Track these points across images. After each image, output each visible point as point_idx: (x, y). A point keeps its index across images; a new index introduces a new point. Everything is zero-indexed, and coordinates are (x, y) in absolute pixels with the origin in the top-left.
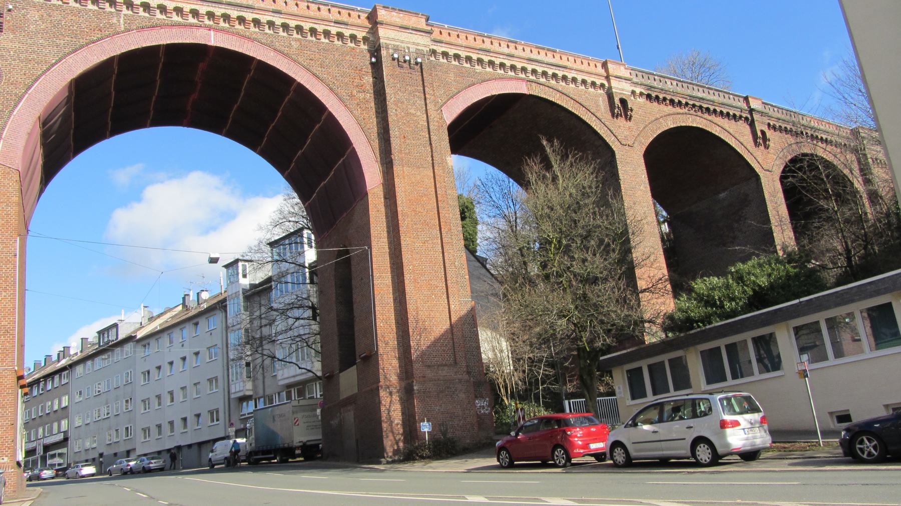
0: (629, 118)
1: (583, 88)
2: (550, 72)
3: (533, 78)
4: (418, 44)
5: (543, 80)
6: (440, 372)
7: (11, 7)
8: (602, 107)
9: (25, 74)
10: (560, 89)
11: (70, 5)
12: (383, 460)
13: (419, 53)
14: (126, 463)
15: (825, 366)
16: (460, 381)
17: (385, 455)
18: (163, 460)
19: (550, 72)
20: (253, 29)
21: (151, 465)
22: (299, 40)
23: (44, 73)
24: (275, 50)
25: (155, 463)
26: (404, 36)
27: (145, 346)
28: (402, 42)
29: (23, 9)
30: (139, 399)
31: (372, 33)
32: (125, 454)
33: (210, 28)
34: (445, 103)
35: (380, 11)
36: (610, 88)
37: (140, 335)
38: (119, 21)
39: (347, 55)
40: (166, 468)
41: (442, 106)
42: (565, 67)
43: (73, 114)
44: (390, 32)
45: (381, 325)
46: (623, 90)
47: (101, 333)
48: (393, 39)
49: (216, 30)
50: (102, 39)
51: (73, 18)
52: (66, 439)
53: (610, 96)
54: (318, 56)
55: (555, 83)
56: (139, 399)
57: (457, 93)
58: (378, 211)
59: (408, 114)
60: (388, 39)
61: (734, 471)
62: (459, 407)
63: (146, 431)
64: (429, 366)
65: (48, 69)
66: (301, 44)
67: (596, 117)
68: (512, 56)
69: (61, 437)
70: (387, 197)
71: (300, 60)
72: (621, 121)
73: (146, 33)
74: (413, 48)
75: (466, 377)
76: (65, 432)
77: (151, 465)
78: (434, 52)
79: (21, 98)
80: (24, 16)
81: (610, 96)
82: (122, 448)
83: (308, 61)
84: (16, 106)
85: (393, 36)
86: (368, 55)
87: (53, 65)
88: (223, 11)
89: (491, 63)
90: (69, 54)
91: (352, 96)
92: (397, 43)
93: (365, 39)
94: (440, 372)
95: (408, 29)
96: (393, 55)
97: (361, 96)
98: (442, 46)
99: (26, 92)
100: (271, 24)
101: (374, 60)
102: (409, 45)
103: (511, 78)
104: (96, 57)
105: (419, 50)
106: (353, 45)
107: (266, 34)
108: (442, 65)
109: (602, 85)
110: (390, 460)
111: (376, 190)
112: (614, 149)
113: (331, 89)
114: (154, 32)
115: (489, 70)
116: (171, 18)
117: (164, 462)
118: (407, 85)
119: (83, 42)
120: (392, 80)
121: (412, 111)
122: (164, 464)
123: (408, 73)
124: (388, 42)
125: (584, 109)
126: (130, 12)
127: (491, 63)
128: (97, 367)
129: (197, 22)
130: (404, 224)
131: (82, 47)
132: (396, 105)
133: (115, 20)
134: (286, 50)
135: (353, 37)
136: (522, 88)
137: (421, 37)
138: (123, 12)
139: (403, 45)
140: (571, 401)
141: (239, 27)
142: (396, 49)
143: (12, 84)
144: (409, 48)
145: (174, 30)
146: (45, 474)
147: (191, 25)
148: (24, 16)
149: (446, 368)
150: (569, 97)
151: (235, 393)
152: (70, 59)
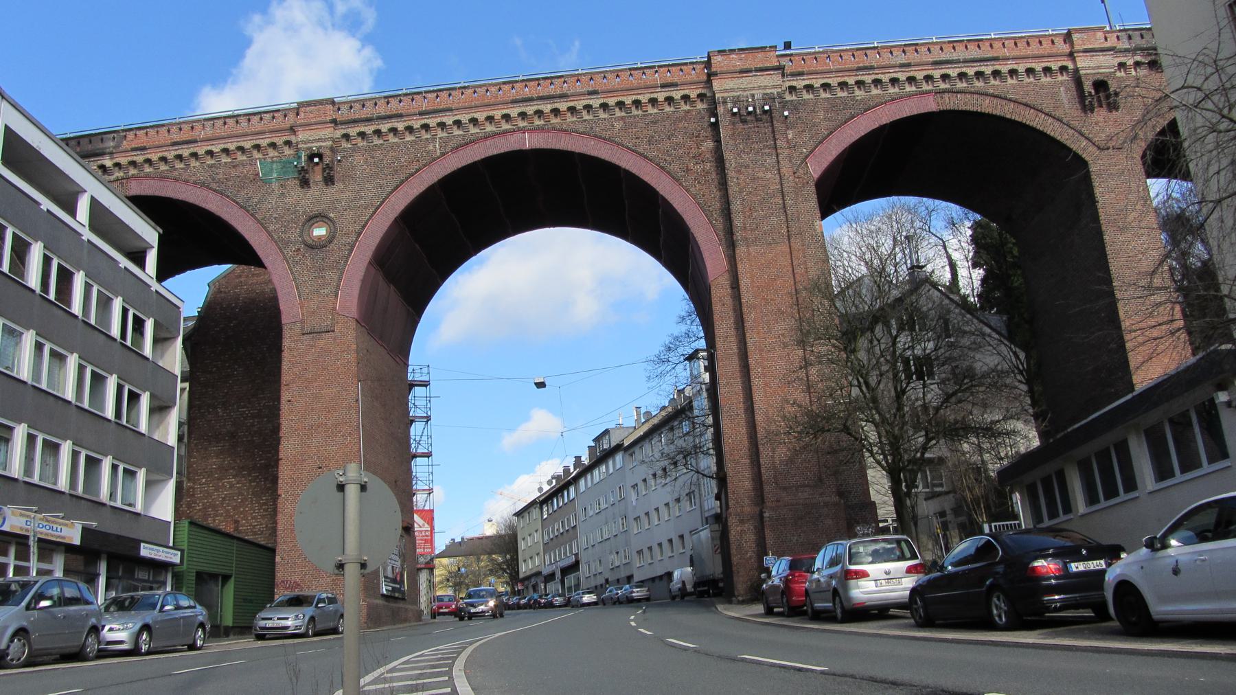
0: (1113, 107)
1: (1032, 79)
2: (971, 72)
3: (943, 86)
4: (765, 88)
5: (961, 85)
6: (800, 494)
7: (339, 158)
8: (1065, 101)
9: (355, 223)
10: (991, 91)
11: (390, 141)
12: (734, 599)
13: (769, 98)
14: (615, 592)
15: (1169, 485)
16: (826, 504)
17: (736, 593)
18: (646, 589)
19: (971, 72)
20: (570, 118)
21: (634, 594)
22: (622, 118)
23: (371, 217)
24: (596, 136)
25: (638, 592)
26: (745, 82)
27: (632, 455)
28: (744, 90)
29: (350, 157)
30: (631, 516)
31: (708, 87)
32: (626, 579)
33: (523, 130)
34: (812, 151)
35: (715, 58)
36: (1076, 70)
37: (626, 443)
38: (435, 147)
39: (681, 121)
40: (652, 597)
41: (807, 157)
42: (996, 59)
43: (417, 245)
44: (727, 81)
45: (730, 441)
46: (1099, 68)
47: (597, 440)
48: (733, 90)
49: (530, 131)
50: (420, 169)
51: (394, 154)
52: (577, 563)
53: (1078, 81)
54: (645, 132)
55: (983, 84)
56: (631, 516)
57: (828, 135)
58: (724, 305)
59: (754, 179)
60: (726, 91)
61: (171, 646)
62: (824, 536)
63: (640, 552)
64: (785, 489)
65: (374, 213)
66: (624, 123)
67: (1054, 118)
68: (908, 65)
69: (573, 559)
70: (734, 286)
71: (625, 142)
72: (1100, 115)
73: (461, 152)
74: (758, 94)
75: (835, 499)
76: (576, 555)
77: (634, 594)
78: (792, 89)
79: (353, 247)
80: (351, 163)
81: (1078, 81)
82: (623, 574)
83: (634, 141)
84: (349, 255)
85: (731, 86)
86: (707, 115)
87: (378, 208)
88: (535, 108)
89: (877, 82)
90: (391, 193)
91: (688, 170)
92: (736, 94)
93: (701, 96)
94: (800, 494)
95: (750, 71)
96: (732, 110)
97: (699, 168)
98: (804, 79)
99: (357, 240)
100: (588, 108)
101: (713, 120)
102: (753, 92)
103: (910, 96)
104: (415, 190)
105: (767, 94)
106: (688, 108)
107: (585, 121)
108: (806, 102)
109: (1063, 69)
110: (740, 598)
111: (720, 279)
112: (1087, 159)
113: (662, 168)
114: (469, 150)
115: (875, 91)
116: (485, 129)
117: (647, 591)
118: (753, 143)
119: (403, 177)
120: (731, 142)
121: (761, 174)
122: (648, 593)
123: (754, 127)
124: (726, 95)
125: (1032, 111)
126: (445, 134)
127: (877, 82)
128: (596, 479)
129: (510, 127)
130: (750, 317)
131: (402, 182)
132: (738, 172)
133: (431, 147)
134: (607, 134)
135: (686, 98)
136: (930, 105)
137: (768, 77)
138: (439, 136)
139: (745, 94)
140: (993, 524)
141: (555, 121)
142: (736, 101)
143: (345, 234)
144: (753, 96)
145: (488, 143)
146: (557, 600)
147: (505, 132)
148: (351, 163)
149: (807, 489)
150: (1005, 99)
151: (709, 510)
152: (392, 198)
